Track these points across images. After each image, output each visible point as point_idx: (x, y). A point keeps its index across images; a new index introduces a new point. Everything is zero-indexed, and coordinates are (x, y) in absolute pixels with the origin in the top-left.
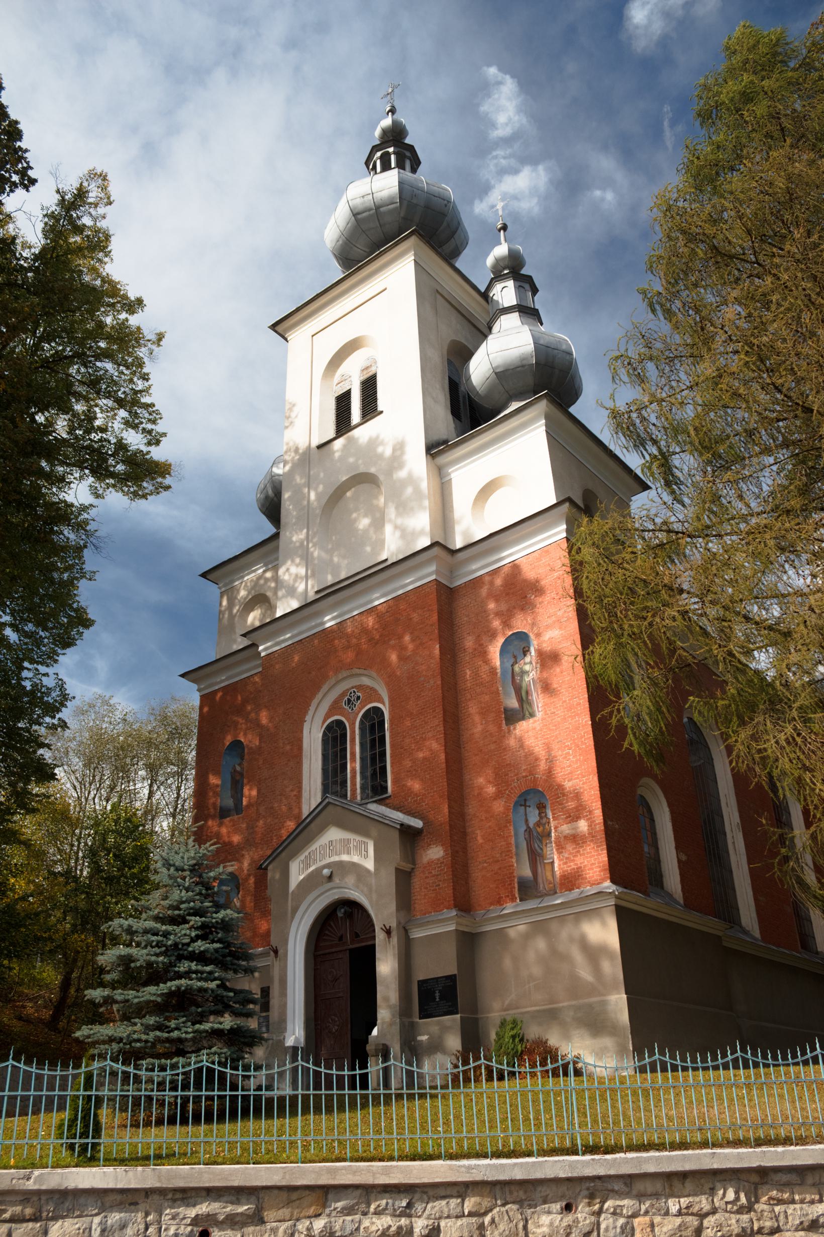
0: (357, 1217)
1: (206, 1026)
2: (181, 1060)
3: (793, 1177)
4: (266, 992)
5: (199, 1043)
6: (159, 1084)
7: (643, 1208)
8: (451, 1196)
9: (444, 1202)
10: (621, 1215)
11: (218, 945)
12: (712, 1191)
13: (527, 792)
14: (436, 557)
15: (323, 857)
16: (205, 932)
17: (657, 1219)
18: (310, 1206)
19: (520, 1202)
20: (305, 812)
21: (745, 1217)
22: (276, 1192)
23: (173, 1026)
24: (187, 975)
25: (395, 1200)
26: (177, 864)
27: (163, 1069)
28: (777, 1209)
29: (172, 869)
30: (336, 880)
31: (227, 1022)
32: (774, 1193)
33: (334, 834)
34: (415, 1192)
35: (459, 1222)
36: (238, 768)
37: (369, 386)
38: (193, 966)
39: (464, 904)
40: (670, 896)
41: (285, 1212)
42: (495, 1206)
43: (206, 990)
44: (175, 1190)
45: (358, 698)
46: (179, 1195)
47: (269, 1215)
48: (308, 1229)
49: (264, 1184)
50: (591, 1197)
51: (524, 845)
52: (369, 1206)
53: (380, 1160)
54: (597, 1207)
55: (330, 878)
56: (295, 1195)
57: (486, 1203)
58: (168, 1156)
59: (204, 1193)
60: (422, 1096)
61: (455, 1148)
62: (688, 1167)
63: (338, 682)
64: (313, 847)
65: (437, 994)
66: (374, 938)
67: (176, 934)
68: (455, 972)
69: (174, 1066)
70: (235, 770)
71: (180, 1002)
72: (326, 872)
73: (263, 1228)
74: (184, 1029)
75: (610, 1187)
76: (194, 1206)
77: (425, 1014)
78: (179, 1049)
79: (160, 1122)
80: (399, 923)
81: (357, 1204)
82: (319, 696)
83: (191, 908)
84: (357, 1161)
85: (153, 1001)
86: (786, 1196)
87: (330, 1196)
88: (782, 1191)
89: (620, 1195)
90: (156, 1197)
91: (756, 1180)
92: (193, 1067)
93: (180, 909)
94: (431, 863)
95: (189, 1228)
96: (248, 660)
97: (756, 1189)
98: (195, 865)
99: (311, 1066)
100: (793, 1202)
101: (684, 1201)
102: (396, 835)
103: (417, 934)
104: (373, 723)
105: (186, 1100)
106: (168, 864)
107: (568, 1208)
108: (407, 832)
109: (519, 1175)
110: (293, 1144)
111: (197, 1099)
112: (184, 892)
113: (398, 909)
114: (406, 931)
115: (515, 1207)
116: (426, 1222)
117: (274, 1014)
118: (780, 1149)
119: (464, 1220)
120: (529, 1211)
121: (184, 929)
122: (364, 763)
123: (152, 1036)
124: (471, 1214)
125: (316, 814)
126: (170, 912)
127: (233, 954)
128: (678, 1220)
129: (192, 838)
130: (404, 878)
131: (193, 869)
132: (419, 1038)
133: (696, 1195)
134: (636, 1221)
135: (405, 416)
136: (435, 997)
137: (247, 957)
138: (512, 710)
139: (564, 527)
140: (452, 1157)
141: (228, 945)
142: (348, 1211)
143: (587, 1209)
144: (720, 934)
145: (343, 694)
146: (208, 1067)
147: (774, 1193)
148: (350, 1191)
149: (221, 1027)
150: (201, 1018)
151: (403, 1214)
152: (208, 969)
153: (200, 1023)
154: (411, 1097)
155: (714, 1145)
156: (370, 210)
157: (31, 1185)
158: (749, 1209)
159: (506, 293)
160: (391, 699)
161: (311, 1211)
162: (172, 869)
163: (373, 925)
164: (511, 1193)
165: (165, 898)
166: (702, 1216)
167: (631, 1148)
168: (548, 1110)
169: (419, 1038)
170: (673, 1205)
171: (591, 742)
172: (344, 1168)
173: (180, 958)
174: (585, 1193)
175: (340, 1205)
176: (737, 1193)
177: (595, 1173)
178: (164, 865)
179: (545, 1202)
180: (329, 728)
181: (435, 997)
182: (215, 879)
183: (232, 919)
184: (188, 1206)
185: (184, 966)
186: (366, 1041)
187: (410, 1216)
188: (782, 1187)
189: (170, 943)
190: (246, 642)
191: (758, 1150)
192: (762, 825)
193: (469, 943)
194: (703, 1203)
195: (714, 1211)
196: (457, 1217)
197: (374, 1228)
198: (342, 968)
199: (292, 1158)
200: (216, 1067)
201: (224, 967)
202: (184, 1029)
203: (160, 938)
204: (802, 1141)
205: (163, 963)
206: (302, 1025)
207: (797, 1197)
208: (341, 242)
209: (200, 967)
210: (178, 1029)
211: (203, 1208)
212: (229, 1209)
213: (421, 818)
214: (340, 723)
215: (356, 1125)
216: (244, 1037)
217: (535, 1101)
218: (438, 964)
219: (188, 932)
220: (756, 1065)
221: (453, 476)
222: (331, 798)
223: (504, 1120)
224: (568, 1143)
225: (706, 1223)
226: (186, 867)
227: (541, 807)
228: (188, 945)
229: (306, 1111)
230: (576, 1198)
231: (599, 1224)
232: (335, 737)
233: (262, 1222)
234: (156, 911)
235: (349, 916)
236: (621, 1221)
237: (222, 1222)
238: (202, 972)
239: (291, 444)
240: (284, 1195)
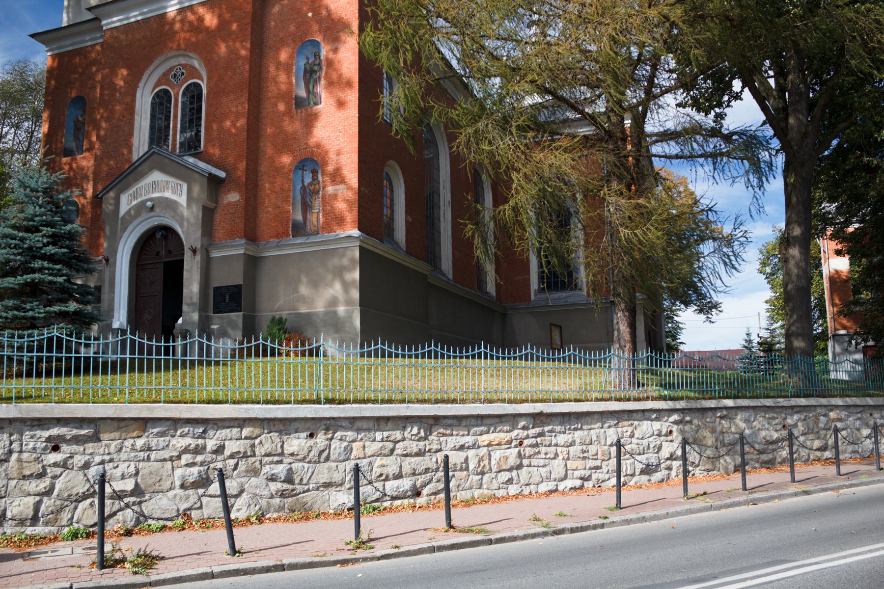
0: (167, 438)
1: (56, 308)
2: (36, 332)
3: (455, 422)
4: (98, 289)
5: (48, 321)
6: (18, 348)
7: (360, 437)
8: (234, 427)
9: (228, 430)
10: (345, 440)
11: (65, 250)
12: (404, 428)
13: (306, 160)
15: (148, 193)
16: (55, 239)
17: (367, 444)
18: (134, 431)
19: (280, 432)
20: (135, 157)
21: (422, 444)
22: (109, 421)
23: (28, 308)
24: (41, 270)
25: (194, 428)
26: (32, 186)
27: (20, 337)
28: (442, 439)
29: (28, 190)
31: (73, 306)
32: (441, 430)
33: (157, 176)
34: (208, 424)
35: (238, 442)
36: (80, 119)
38: (46, 264)
39: (252, 237)
40: (397, 244)
41: (116, 434)
42: (263, 433)
43: (55, 283)
44: (33, 419)
45: (183, 74)
46: (35, 423)
47: (103, 436)
48: (132, 445)
49: (101, 416)
50: (327, 430)
51: (299, 197)
52: (176, 431)
53: (185, 403)
54: (330, 436)
55: (152, 209)
56: (123, 424)
57: (257, 431)
58: (26, 398)
59: (55, 422)
60: (217, 363)
61: (237, 397)
62: (391, 414)
63: (167, 59)
64: (140, 185)
65: (227, 298)
66: (183, 255)
67: (30, 240)
68: (241, 282)
69: (29, 336)
70: (78, 120)
71: (33, 291)
72: (149, 204)
73: (100, 444)
74: (37, 310)
75: (339, 424)
76: (48, 430)
77: (217, 310)
78: (33, 324)
79: (19, 375)
80: (202, 245)
81: (168, 430)
82: (151, 68)
83: (44, 221)
84: (168, 403)
85: (12, 288)
86: (448, 432)
87: (148, 425)
88: (446, 429)
89: (345, 429)
90: (18, 424)
91: (432, 423)
92: (46, 336)
93: (34, 221)
94: (229, 204)
95: (44, 444)
96: (90, 31)
97: (431, 428)
98: (47, 188)
99: (137, 338)
100: (452, 435)
101: (386, 434)
102: (205, 180)
103: (215, 254)
104: (193, 94)
105: (40, 360)
106: (23, 185)
107: (311, 436)
108: (213, 180)
109: (280, 415)
110: (122, 391)
111: (49, 359)
112: (37, 208)
113: (203, 235)
114: (208, 252)
115: (276, 434)
116: (215, 442)
117: (104, 305)
118: (449, 405)
119: (242, 441)
120: (286, 437)
121: (37, 237)
122: (183, 126)
123: (10, 314)
124: (246, 438)
125: (143, 160)
126: (25, 223)
127: (78, 259)
128: (381, 444)
129: (45, 167)
130: (208, 215)
131: (46, 192)
132: (213, 327)
133: (394, 430)
134: (354, 445)
136: (225, 299)
137: (87, 261)
138: (301, 98)
140: (234, 402)
141: (72, 250)
142: (162, 434)
143: (324, 437)
144: (427, 273)
145: (171, 69)
146: (57, 337)
147: (441, 430)
148: (163, 422)
149: (67, 309)
150: (50, 303)
151: (199, 437)
152: (58, 267)
153: (50, 306)
154: (209, 363)
155: (409, 402)
158: (426, 438)
160: (209, 79)
161: (135, 434)
162: (28, 190)
163: (183, 245)
164: (274, 426)
165: (22, 211)
166: (396, 442)
167: (356, 401)
168: (303, 376)
169: (213, 327)
170: (379, 435)
171: (356, 130)
172: (160, 407)
173: (34, 258)
174: (324, 427)
175: (155, 430)
176: (419, 429)
177: (331, 416)
178: (20, 186)
179: (296, 432)
181: (225, 299)
182: (63, 200)
183: (77, 232)
184: (43, 429)
185: (37, 264)
186: (174, 327)
187: (205, 438)
188: (446, 427)
189: (26, 246)
190: (89, 16)
191: (436, 406)
192: (468, 200)
193: (253, 263)
194: (398, 435)
195: (404, 439)
196: (237, 439)
197: (179, 445)
198: (157, 276)
199: (121, 400)
200: (64, 336)
201: (68, 265)
202: (37, 310)
203: (17, 242)
204: (463, 401)
205: (20, 261)
206: (126, 314)
207: (454, 433)
209: (51, 265)
210: (32, 310)
211: (55, 431)
212: (75, 432)
213: (224, 170)
215: (167, 381)
216: (85, 317)
217: (295, 371)
218: (229, 276)
219: (41, 239)
220: (443, 356)
222: (156, 149)
223: (273, 381)
224: (315, 397)
225: (398, 446)
226: (40, 189)
227: (314, 172)
228: (41, 248)
229: (132, 370)
230: (317, 430)
231: (330, 446)
232: (161, 102)
233: (99, 440)
234: (13, 222)
235: (165, 237)
236: (345, 444)
237: (69, 440)
238: (53, 270)
240: (116, 424)
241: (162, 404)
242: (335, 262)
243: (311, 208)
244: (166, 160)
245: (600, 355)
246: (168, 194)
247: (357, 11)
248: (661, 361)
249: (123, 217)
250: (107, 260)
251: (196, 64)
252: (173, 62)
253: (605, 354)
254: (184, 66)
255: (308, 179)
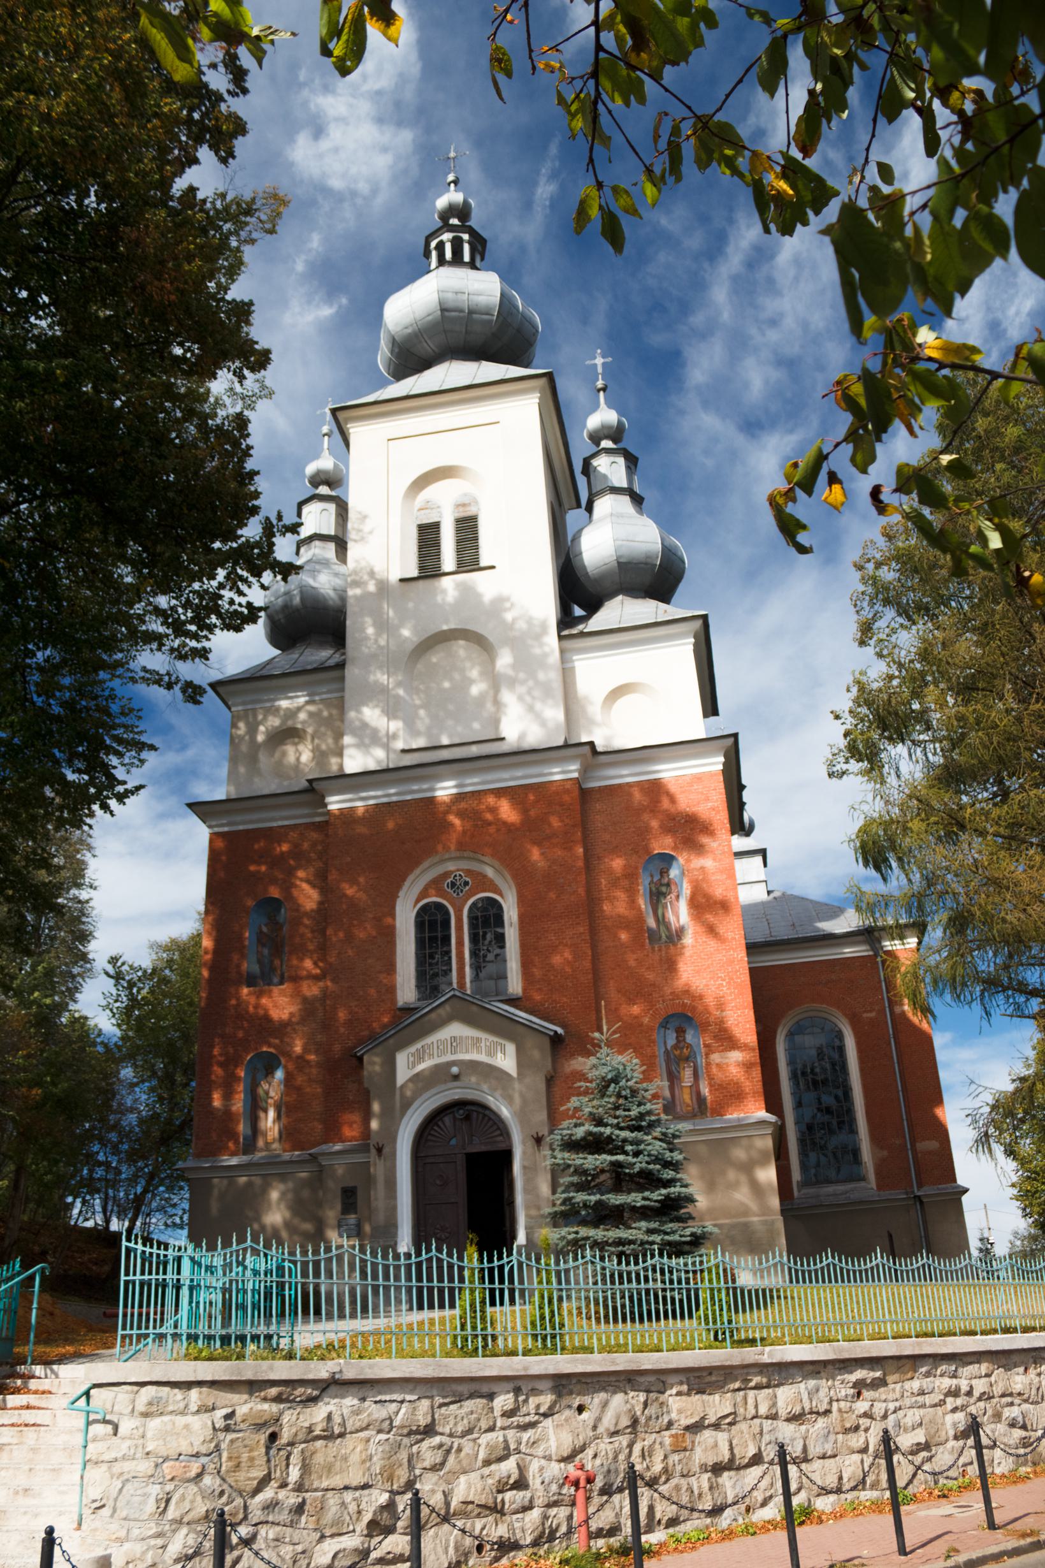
14: (583, 756)
30: (465, 1080)
37: (468, 528)
45: (466, 883)
70: (261, 932)
72: (455, 1070)
82: (417, 871)
135: (519, 578)
139: (722, 759)
142: (928, 1374)
156: (462, 311)
157: (766, 1359)
159: (611, 468)
180: (424, 910)
208: (409, 331)
211: (859, 1374)
214: (439, 907)
221: (577, 664)
239: (363, 564)
241: (978, 1337)
242: (739, 1154)
243: (680, 1079)
244: (474, 1008)
245: (490, 1261)
246: (482, 1057)
247: (726, 821)
248: (803, 1272)
249: (402, 1086)
250: (379, 1150)
251: (490, 872)
252: (451, 866)
253: (500, 1258)
254: (469, 872)
255: (671, 1041)
